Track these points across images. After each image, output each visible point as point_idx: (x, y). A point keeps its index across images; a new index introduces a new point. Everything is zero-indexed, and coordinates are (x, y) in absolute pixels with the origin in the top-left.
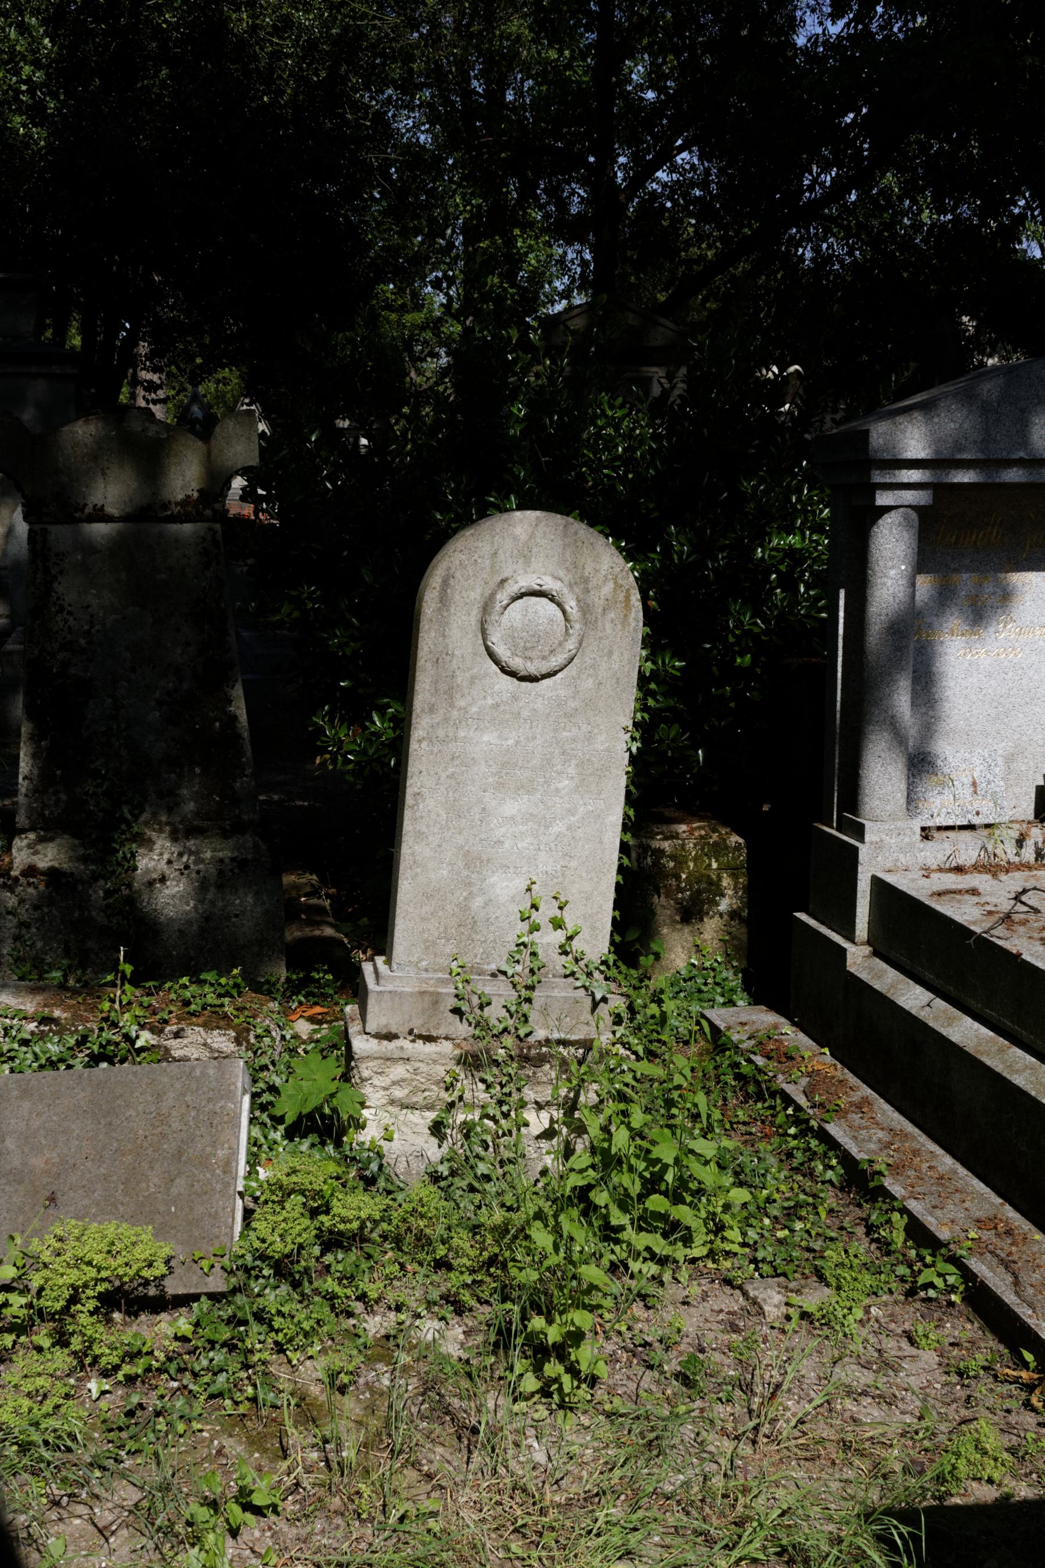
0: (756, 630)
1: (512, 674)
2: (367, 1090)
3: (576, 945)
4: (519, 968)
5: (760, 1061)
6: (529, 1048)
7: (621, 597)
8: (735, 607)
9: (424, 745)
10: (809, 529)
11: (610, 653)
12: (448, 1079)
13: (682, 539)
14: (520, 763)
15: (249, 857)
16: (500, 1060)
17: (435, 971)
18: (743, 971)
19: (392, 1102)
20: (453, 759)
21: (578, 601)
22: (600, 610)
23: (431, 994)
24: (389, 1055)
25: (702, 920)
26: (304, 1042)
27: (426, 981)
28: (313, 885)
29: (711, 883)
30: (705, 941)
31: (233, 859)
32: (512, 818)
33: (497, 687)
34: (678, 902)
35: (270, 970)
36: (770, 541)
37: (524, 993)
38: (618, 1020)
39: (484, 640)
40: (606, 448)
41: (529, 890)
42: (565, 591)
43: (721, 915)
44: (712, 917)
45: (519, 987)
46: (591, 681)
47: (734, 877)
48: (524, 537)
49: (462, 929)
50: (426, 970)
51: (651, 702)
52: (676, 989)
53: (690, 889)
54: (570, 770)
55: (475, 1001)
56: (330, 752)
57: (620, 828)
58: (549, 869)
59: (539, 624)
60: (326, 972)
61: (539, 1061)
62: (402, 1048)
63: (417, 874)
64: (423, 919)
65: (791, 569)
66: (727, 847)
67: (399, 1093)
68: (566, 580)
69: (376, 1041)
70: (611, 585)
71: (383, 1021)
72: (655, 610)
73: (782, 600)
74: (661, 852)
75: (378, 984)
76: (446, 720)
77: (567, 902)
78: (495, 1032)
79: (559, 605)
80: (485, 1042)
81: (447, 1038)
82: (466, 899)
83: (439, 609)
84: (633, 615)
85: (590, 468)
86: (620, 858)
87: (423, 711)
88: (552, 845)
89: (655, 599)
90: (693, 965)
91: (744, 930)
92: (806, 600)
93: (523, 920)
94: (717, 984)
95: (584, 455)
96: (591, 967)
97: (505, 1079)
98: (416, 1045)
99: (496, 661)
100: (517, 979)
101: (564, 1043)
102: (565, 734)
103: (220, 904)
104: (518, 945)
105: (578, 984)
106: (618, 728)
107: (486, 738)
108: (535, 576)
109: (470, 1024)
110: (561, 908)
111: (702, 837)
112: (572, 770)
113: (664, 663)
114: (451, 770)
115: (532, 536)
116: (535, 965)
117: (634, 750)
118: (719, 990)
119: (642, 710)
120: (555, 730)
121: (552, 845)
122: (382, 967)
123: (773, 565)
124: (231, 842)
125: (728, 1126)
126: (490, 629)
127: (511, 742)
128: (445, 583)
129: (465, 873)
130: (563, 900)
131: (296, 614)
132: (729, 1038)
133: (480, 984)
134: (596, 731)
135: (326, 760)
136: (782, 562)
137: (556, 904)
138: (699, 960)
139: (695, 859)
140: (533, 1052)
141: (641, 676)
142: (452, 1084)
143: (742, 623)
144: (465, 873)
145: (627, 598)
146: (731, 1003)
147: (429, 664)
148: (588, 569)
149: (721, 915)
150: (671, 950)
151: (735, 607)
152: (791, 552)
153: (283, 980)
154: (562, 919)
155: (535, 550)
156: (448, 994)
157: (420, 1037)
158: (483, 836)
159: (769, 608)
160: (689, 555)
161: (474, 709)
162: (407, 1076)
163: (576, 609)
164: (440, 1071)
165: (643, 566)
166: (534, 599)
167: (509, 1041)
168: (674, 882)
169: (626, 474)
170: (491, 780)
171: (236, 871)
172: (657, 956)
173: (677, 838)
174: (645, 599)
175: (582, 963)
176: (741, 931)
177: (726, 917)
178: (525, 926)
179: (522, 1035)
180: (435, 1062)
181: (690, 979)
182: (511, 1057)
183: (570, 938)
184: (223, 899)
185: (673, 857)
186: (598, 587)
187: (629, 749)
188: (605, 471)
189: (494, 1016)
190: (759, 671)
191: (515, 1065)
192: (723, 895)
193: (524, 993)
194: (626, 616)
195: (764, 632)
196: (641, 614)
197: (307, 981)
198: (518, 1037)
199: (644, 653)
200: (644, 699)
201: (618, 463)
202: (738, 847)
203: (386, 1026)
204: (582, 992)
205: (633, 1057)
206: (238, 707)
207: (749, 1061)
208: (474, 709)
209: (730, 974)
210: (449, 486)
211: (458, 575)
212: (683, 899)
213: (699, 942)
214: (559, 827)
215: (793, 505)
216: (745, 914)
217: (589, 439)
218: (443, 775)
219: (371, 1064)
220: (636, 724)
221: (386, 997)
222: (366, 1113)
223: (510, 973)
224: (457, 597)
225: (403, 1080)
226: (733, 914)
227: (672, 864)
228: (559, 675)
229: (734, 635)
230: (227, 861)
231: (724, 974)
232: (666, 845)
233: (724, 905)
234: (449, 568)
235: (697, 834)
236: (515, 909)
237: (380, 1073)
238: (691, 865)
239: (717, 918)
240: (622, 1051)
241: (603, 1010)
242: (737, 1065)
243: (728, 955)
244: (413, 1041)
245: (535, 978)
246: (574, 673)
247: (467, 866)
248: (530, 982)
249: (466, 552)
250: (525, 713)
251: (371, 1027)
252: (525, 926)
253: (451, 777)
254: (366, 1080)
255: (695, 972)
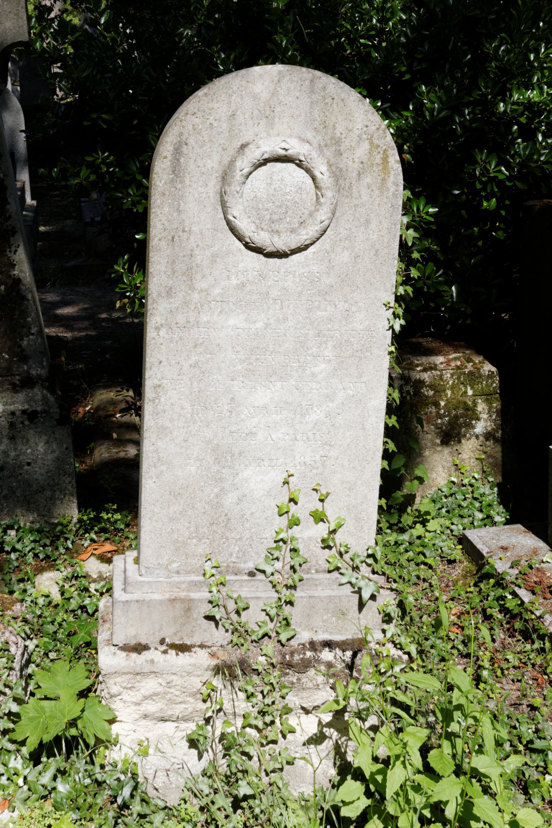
0: (501, 177)
1: (258, 250)
2: (117, 706)
3: (339, 537)
4: (278, 565)
5: (525, 595)
6: (292, 654)
7: (378, 159)
8: (481, 157)
9: (162, 332)
10: (546, 83)
11: (368, 222)
12: (205, 691)
13: (432, 95)
14: (271, 348)
15: (39, 409)
16: (260, 669)
17: (187, 573)
18: (499, 485)
19: (146, 716)
20: (195, 346)
21: (330, 165)
22: (354, 175)
23: (182, 600)
24: (138, 670)
25: (459, 442)
26: (94, 581)
27: (177, 585)
28: (127, 402)
29: (467, 408)
30: (463, 460)
31: (24, 412)
32: (265, 407)
33: (241, 265)
34: (437, 426)
35: (62, 511)
36: (511, 96)
37: (286, 594)
38: (388, 619)
39: (225, 213)
40: (362, 19)
41: (286, 483)
42: (314, 154)
43: (477, 437)
44: (469, 439)
45: (279, 588)
46: (346, 254)
47: (488, 402)
48: (265, 95)
49: (214, 527)
50: (178, 572)
51: (414, 273)
52: (439, 506)
53: (449, 415)
54: (326, 353)
55: (231, 606)
56: (128, 297)
57: (384, 411)
58: (308, 460)
59: (286, 194)
60: (116, 511)
61: (306, 665)
62: (152, 661)
63: (162, 472)
64: (171, 519)
65: (530, 120)
66: (481, 376)
67: (151, 707)
68: (315, 142)
69: (124, 654)
70: (366, 146)
71: (131, 632)
72: (409, 163)
73: (525, 148)
74: (420, 383)
75: (124, 590)
76: (186, 304)
77: (328, 494)
78: (254, 637)
79: (308, 171)
80: (244, 649)
81: (202, 646)
82: (217, 496)
83: (172, 181)
84: (392, 179)
85: (348, 38)
86: (385, 443)
87: (159, 295)
88: (310, 434)
89: (410, 153)
90: (453, 482)
91: (499, 448)
92: (545, 148)
93: (281, 515)
94: (475, 499)
95: (342, 26)
96: (357, 562)
97: (267, 689)
98: (168, 657)
99: (240, 238)
100: (277, 578)
101: (329, 645)
102: (319, 313)
103: (13, 454)
104: (276, 542)
105: (344, 580)
106: (379, 304)
107: (232, 322)
108: (279, 139)
109: (227, 631)
110: (322, 501)
111: (458, 368)
112: (328, 353)
113: (418, 209)
114: (194, 359)
115: (274, 94)
116: (296, 562)
117: (397, 328)
118: (477, 505)
119: (404, 283)
120: (309, 310)
121: (310, 434)
122: (132, 567)
123: (514, 118)
124: (21, 396)
125: (499, 673)
126: (230, 201)
127: (260, 325)
128: (177, 152)
129: (215, 468)
130: (324, 492)
131: (93, 178)
132: (492, 567)
133: (236, 587)
134: (354, 309)
135: (125, 304)
136: (522, 115)
137: (317, 496)
138: (458, 477)
139: (452, 388)
140: (297, 657)
141: (403, 245)
142: (209, 696)
143: (488, 171)
144: (215, 468)
145: (385, 160)
146: (489, 521)
147: (163, 243)
148: (340, 129)
149: (477, 437)
150: (432, 469)
151: (481, 157)
152: (529, 106)
153: (75, 520)
154: (323, 513)
155: (278, 109)
156: (200, 600)
157: (173, 646)
158: (233, 428)
159: (512, 157)
160: (440, 112)
161: (217, 291)
162: (160, 689)
163: (327, 174)
164: (196, 683)
165: (397, 123)
166: (279, 166)
167: (269, 647)
168: (433, 409)
169: (380, 43)
170: (239, 367)
171: (27, 423)
172: (421, 480)
173: (436, 369)
174: (401, 152)
175: (347, 557)
176: (496, 450)
177: (481, 438)
178: (284, 521)
179: (284, 641)
180: (189, 674)
181: (451, 495)
182: (272, 665)
183: (334, 531)
184: (15, 449)
185: (431, 387)
186: (351, 149)
187: (392, 328)
188: (362, 41)
189: (253, 620)
190: (503, 213)
191: (277, 673)
192: (478, 419)
193: (286, 594)
194: (383, 180)
195: (509, 178)
196: (401, 177)
197: (98, 519)
198: (279, 641)
199: (405, 220)
200: (407, 269)
201: (373, 33)
202: (491, 375)
203: (135, 637)
204: (349, 588)
205: (406, 657)
206: (21, 271)
207: (515, 595)
208: (217, 291)
209: (487, 490)
210: (219, 56)
211: (192, 141)
212: (442, 424)
213: (457, 462)
214: (316, 415)
215: (531, 63)
216: (499, 434)
217: (346, 14)
218: (186, 365)
219: (119, 680)
220: (398, 299)
221: (134, 606)
222: (115, 728)
223: (269, 570)
224: (192, 166)
225: (156, 694)
226: (488, 436)
227: (431, 393)
228: (311, 249)
229: (481, 182)
230: (18, 413)
231: (482, 491)
232: (426, 376)
233: (480, 427)
234: (181, 134)
235: (453, 364)
236: (271, 505)
237: (130, 688)
238: (449, 393)
239: (473, 439)
240: (395, 652)
241: (372, 608)
242: (503, 598)
243: (484, 472)
244: (165, 652)
245: (296, 577)
246: (327, 246)
247: (217, 461)
248: (290, 582)
249: (199, 114)
250: (274, 293)
251: (120, 639)
252: (284, 521)
253: (194, 366)
254: (115, 696)
255: (455, 489)
